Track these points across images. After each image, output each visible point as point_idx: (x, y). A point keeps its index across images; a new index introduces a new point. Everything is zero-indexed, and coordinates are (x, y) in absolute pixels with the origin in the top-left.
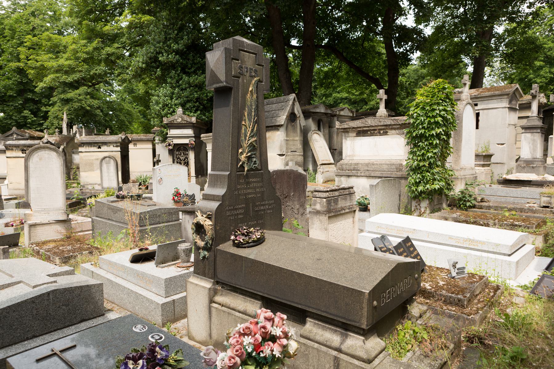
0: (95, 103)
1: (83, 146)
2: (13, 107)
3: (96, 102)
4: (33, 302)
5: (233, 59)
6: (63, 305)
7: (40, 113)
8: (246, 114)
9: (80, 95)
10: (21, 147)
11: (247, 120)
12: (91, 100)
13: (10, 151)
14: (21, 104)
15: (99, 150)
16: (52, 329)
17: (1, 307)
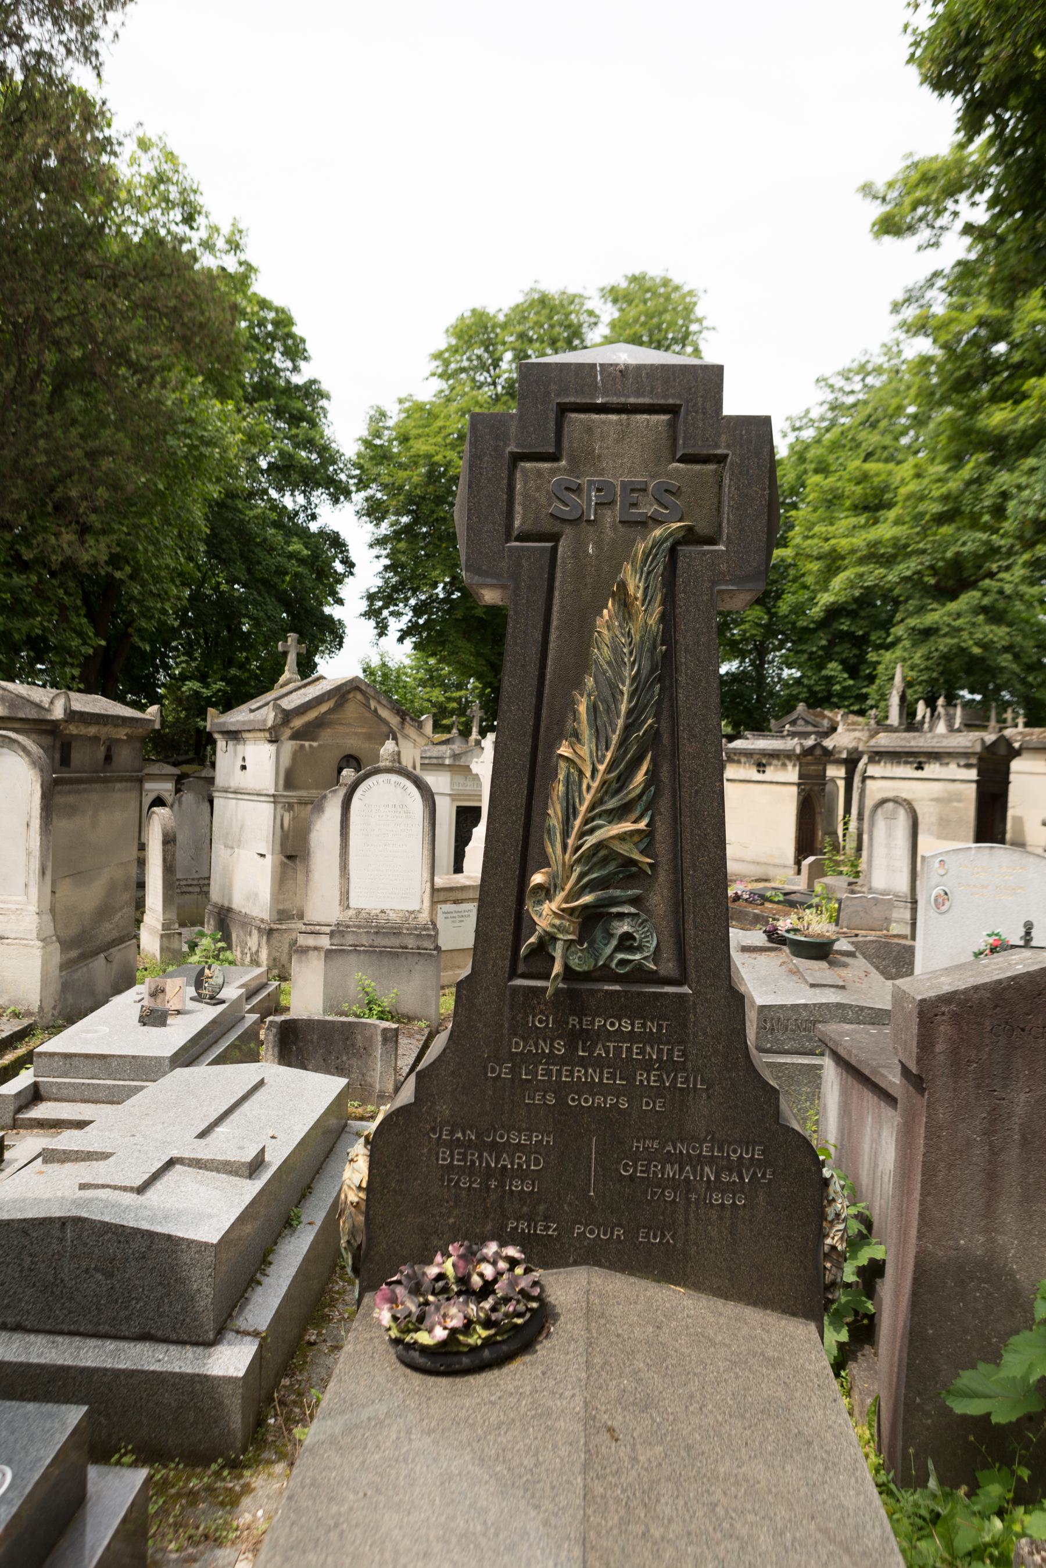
0: (999, 633)
1: (879, 762)
2: (806, 656)
3: (1002, 631)
4: (26, 1233)
5: (517, 458)
6: (96, 1269)
7: (863, 667)
8: (582, 708)
9: (959, 615)
10: (756, 757)
11: (586, 732)
12: (987, 628)
13: (735, 765)
14: (823, 648)
15: (919, 774)
16: (65, 1328)
17: (6, 1216)
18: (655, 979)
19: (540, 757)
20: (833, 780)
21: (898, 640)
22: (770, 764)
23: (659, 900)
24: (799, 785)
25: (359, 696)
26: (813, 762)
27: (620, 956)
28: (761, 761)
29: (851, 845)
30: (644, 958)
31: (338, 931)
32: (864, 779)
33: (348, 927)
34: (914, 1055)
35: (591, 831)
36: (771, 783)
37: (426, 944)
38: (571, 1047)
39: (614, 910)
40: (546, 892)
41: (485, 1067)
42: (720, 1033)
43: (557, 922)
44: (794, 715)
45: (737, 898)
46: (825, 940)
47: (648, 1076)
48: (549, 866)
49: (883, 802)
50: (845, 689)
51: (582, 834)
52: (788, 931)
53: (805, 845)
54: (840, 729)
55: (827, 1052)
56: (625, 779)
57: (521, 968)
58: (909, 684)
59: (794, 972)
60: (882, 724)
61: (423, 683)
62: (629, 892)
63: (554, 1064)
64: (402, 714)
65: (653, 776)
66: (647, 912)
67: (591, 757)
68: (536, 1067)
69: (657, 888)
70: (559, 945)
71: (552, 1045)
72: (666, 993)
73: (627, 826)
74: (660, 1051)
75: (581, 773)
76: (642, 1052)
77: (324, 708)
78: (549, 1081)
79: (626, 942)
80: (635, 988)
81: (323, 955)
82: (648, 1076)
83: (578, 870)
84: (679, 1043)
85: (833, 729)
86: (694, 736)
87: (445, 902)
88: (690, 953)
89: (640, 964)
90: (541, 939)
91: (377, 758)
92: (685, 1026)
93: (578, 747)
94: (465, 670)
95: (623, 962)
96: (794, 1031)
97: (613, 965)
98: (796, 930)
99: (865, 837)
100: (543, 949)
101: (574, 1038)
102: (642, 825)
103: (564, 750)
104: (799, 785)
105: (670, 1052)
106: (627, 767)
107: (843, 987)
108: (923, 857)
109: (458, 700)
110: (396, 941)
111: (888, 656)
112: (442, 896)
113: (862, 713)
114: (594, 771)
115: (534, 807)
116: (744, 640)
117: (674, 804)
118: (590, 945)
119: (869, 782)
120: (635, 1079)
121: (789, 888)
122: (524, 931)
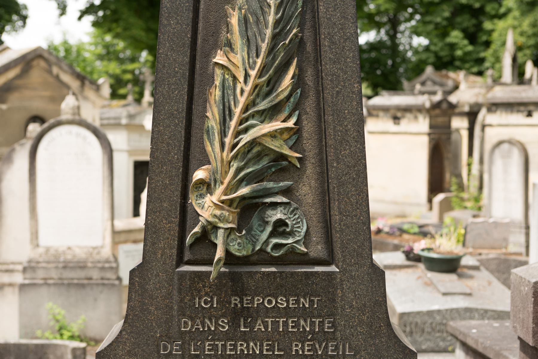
1: (495, 112)
8: (234, 21)
14: (447, 19)
15: (529, 121)
18: (305, 260)
19: (198, 66)
20: (458, 130)
21: (509, 11)
22: (403, 117)
23: (307, 189)
24: (429, 134)
25: (42, 63)
26: (441, 113)
27: (274, 241)
28: (397, 115)
29: (474, 183)
30: (297, 242)
31: (29, 268)
32: (484, 127)
33: (38, 262)
34: (531, 330)
35: (246, 130)
36: (405, 133)
37: (111, 275)
38: (234, 323)
39: (268, 200)
40: (207, 186)
41: (158, 346)
42: (365, 305)
43: (218, 212)
44: (423, 77)
45: (379, 231)
46: (454, 256)
47: (303, 346)
48: (209, 163)
49: (499, 144)
50: (466, 54)
51: (238, 134)
52: (423, 250)
53: (436, 185)
54: (463, 86)
55: (458, 345)
56: (273, 84)
57: (187, 256)
58: (519, 48)
59: (430, 284)
60: (497, 81)
61: (101, 57)
62: (281, 184)
63: (219, 340)
64: (81, 78)
65: (299, 81)
66: (298, 201)
67: (244, 64)
68: (203, 343)
69: (305, 179)
70: (221, 233)
71: (217, 324)
72: (316, 273)
73: (276, 125)
74: (313, 324)
75: (235, 78)
76: (297, 325)
77: (11, 74)
78: (216, 355)
79: (280, 229)
80: (289, 269)
81: (17, 290)
82: (303, 346)
83: (235, 165)
84: (329, 316)
85: (456, 87)
86: (334, 43)
87: (125, 242)
88: (336, 236)
89: (293, 248)
90: (204, 228)
91: (58, 112)
92: (334, 300)
93: (231, 56)
94: (138, 45)
95: (277, 246)
96: (429, 333)
97: (269, 249)
98: (429, 250)
99: (486, 177)
100: (205, 238)
101: (237, 315)
102: (291, 124)
103: (219, 58)
104: (429, 134)
105: (321, 323)
106: (275, 72)
107: (470, 295)
108: (534, 185)
109: (132, 72)
110: (82, 274)
111: (501, 24)
112: (123, 237)
113: (480, 74)
114: (247, 76)
115: (194, 112)
116: (379, 13)
117: (318, 104)
118: (249, 231)
119: (488, 130)
120: (291, 350)
121: (422, 222)
122: (189, 223)
